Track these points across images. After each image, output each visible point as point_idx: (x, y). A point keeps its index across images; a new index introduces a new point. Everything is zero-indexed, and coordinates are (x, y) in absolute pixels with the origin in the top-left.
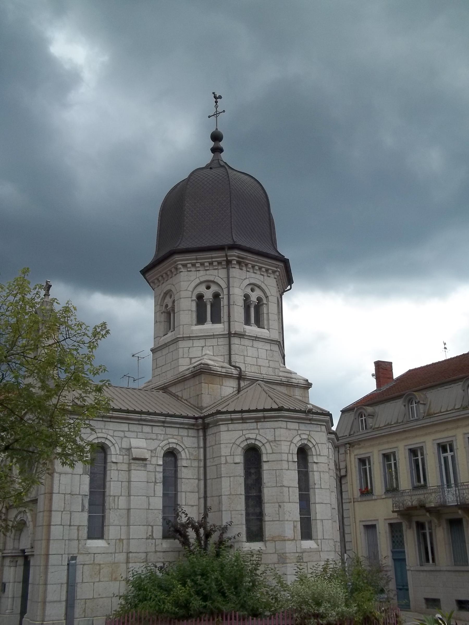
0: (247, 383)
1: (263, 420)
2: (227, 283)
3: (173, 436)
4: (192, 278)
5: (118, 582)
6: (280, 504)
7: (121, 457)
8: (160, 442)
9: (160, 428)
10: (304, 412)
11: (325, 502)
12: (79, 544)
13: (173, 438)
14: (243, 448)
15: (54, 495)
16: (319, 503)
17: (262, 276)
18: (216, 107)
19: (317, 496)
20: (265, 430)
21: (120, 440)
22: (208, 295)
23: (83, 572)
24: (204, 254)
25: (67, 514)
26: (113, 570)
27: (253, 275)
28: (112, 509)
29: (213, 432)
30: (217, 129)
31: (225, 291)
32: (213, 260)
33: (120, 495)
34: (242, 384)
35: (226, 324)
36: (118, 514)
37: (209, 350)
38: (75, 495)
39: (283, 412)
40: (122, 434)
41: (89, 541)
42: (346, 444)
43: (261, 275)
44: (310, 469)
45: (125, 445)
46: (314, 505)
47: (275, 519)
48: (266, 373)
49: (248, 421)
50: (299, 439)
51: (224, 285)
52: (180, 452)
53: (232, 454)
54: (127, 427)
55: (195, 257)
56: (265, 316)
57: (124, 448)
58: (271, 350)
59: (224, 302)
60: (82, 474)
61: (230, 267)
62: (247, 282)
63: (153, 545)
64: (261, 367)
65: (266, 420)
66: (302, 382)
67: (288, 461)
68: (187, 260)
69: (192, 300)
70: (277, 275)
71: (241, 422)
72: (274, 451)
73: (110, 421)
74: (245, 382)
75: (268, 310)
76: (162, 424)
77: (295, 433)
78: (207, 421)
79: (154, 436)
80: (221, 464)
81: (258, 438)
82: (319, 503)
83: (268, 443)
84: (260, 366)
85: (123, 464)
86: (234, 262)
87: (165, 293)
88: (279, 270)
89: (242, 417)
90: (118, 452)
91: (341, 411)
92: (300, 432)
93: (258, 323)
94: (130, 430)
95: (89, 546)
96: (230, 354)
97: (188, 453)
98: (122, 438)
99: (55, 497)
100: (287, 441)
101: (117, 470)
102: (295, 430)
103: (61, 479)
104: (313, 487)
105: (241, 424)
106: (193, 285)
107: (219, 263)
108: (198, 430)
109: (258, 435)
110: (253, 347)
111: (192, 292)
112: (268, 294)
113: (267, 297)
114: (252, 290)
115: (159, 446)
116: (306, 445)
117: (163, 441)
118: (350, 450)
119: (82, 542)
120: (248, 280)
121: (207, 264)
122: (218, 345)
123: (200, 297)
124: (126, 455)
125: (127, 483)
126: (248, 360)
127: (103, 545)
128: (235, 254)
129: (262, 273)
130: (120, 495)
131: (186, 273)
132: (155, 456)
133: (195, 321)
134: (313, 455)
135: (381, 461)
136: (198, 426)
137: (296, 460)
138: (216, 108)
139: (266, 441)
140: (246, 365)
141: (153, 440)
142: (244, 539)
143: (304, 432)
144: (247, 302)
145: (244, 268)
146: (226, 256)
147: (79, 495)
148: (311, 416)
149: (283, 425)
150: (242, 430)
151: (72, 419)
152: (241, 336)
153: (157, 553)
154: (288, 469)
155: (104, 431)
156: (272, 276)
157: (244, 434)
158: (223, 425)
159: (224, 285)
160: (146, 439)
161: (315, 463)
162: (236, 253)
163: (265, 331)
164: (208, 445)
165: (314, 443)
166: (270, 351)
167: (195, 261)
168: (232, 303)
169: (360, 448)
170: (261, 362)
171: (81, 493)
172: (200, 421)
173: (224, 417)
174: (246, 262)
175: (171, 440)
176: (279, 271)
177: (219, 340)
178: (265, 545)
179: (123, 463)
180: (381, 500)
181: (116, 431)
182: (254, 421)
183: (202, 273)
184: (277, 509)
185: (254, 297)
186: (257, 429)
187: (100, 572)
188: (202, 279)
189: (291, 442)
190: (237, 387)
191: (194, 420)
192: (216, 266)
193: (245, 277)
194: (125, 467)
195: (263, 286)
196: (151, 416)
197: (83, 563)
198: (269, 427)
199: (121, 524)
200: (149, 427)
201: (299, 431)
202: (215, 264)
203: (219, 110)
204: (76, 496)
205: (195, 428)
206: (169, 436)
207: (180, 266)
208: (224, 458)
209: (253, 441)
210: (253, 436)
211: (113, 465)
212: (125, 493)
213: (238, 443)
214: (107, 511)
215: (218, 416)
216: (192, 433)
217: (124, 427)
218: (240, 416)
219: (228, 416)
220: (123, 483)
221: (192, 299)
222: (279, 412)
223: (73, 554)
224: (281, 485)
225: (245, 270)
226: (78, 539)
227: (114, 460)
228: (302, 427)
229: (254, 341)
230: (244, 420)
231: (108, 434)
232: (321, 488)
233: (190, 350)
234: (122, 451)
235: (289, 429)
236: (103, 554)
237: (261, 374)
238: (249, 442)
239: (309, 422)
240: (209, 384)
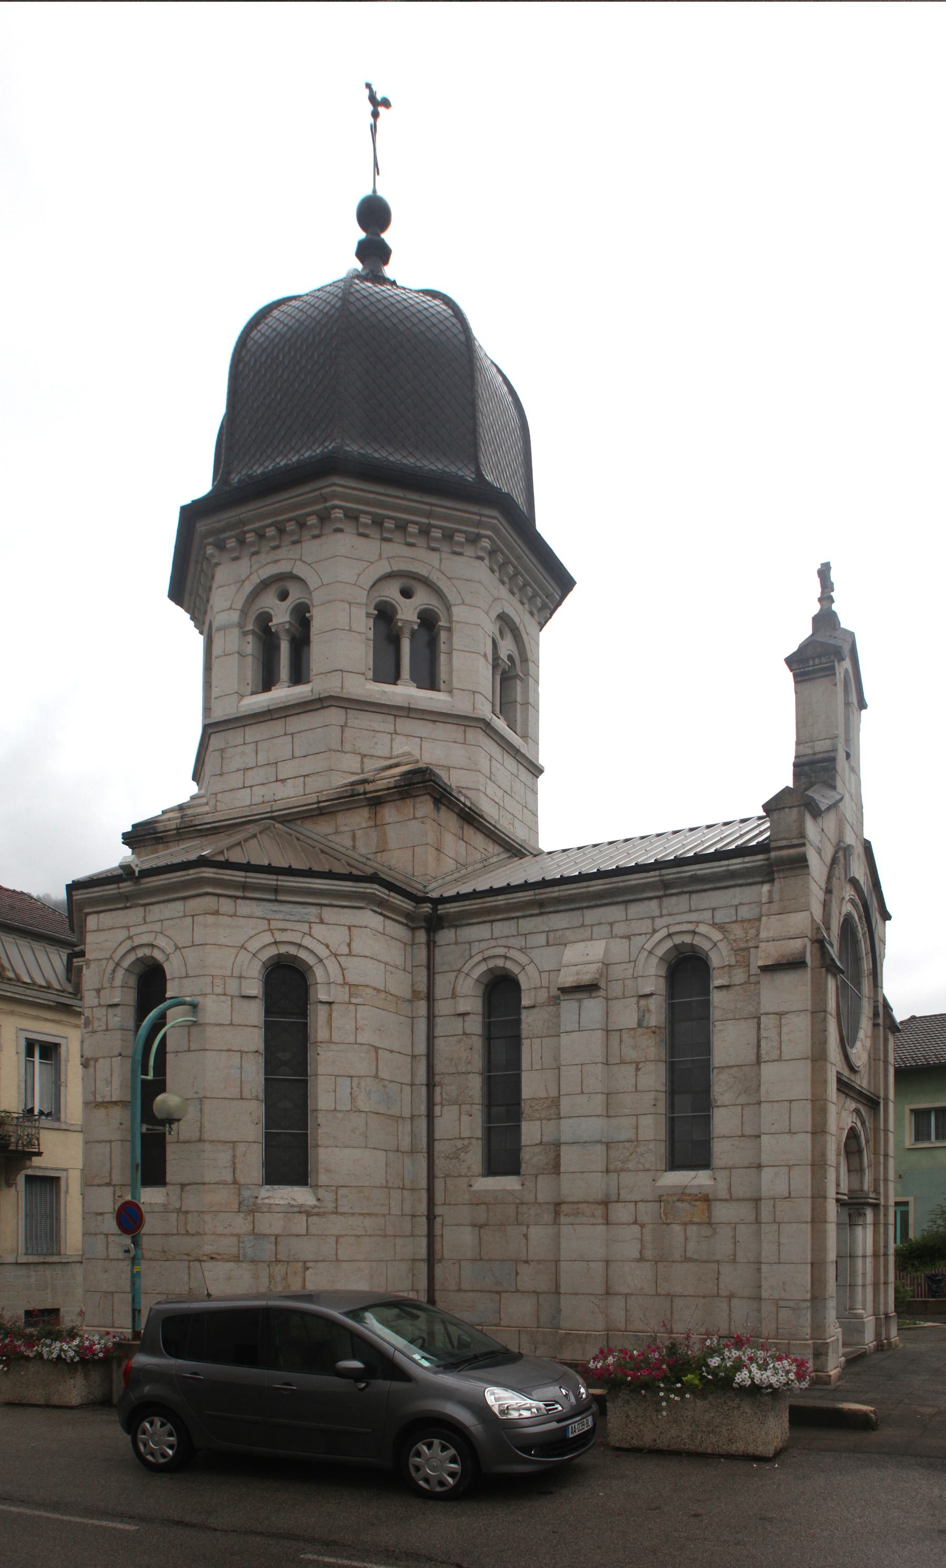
14: (661, 958)
22: (281, 616)
30: (374, 191)
50: (267, 938)
68: (367, 502)
69: (245, 634)
77: (263, 925)
78: (443, 909)
80: (126, 970)
111: (244, 612)
156: (469, 551)
172: (426, 908)
195: (435, 577)
225: (378, 536)
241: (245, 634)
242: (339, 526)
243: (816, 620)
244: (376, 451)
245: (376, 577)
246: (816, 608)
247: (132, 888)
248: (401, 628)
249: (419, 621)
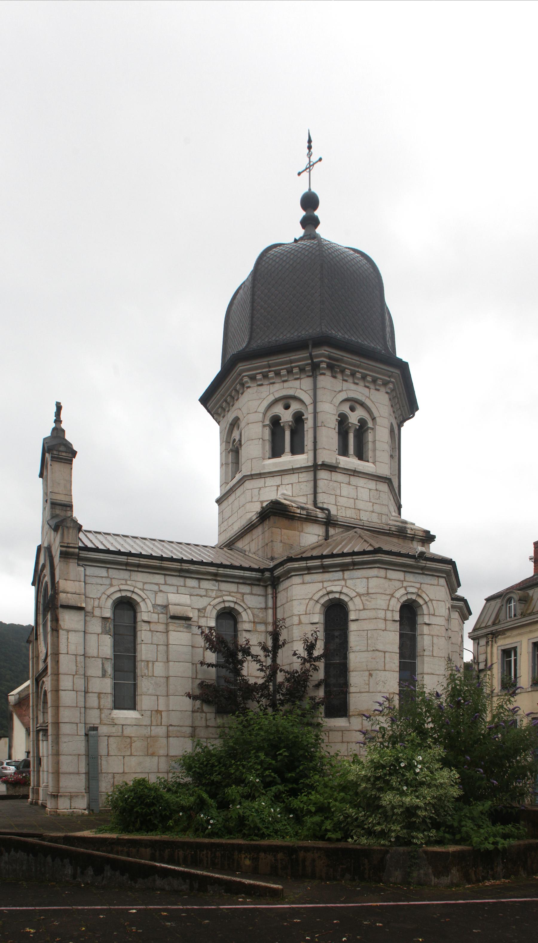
0: (338, 530)
1: (352, 568)
2: (312, 397)
3: (230, 594)
4: (264, 395)
5: (157, 758)
6: (370, 672)
7: (156, 616)
8: (211, 599)
9: (211, 582)
10: (413, 557)
11: (438, 673)
12: (101, 713)
13: (230, 595)
14: (322, 605)
15: (61, 657)
16: (428, 674)
17: (367, 390)
18: (310, 155)
19: (425, 665)
20: (354, 580)
21: (154, 595)
22: (287, 417)
23: (108, 745)
24: (280, 357)
25: (80, 678)
26: (148, 744)
27: (353, 387)
28: (145, 675)
29: (284, 588)
30: (310, 189)
31: (311, 408)
32: (293, 365)
33: (155, 660)
34: (332, 531)
35: (311, 454)
36: (153, 682)
37: (287, 490)
38: (92, 657)
39: (380, 555)
40: (156, 588)
41: (116, 712)
42: (488, 634)
43: (366, 386)
44: (418, 632)
45: (160, 600)
46: (421, 676)
47: (363, 690)
48: (368, 519)
49: (330, 570)
50: (403, 591)
51: (307, 399)
52: (239, 613)
53: (308, 612)
54: (163, 579)
55: (266, 363)
56: (370, 445)
57: (159, 605)
58: (377, 490)
59: (309, 425)
60: (101, 634)
61: (318, 373)
62: (343, 396)
63: (203, 719)
64: (361, 511)
65: (355, 567)
66: (421, 534)
67: (385, 620)
70: (390, 388)
71: (321, 571)
72: (366, 607)
73: (138, 571)
74: (337, 529)
75: (375, 436)
76: (214, 578)
77: (398, 584)
78: (277, 573)
79: (203, 592)
81: (345, 590)
82: (428, 674)
83: (358, 597)
84: (359, 510)
85: (158, 624)
86: (324, 365)
87: (231, 424)
88: (393, 380)
89: (322, 564)
90: (151, 609)
91: (485, 600)
92: (405, 584)
93: (360, 455)
94: (168, 583)
95: (115, 716)
96: (315, 493)
97: (251, 615)
98: (156, 593)
99: (63, 659)
100: (385, 594)
101: (150, 630)
102: (399, 580)
103: (69, 637)
104: (421, 654)
105: (320, 575)
106: (265, 404)
107: (302, 370)
108: (266, 587)
109: (344, 588)
110: (349, 484)
111: (265, 414)
112: (376, 414)
113: (374, 419)
114: (352, 409)
115: (209, 604)
116: (415, 601)
117: (215, 598)
118: (492, 641)
119: (106, 712)
120: (344, 393)
121: (284, 372)
122: (299, 482)
123: (276, 422)
124: (162, 613)
125: (165, 647)
126: (342, 501)
127: (134, 717)
128: (323, 352)
129: (367, 384)
130: (155, 660)
131: (255, 389)
132: (204, 617)
133: (268, 454)
134: (423, 614)
135: (531, 650)
136: (266, 582)
137: (398, 618)
138: (309, 158)
139: (355, 594)
140: (339, 508)
141: (201, 596)
142: (323, 715)
143: (413, 584)
144: (344, 426)
145: (339, 376)
146: (311, 357)
147: (98, 657)
148: (423, 563)
149: (382, 573)
150: (323, 582)
151: (82, 566)
152: (332, 468)
153: (209, 728)
154: (385, 630)
155: (129, 582)
156: (383, 389)
157: (325, 586)
158: (297, 577)
159: (307, 399)
160: (191, 595)
161: (426, 624)
162: (324, 351)
163: (370, 465)
164: (279, 604)
165: (427, 599)
166: (375, 491)
167: (267, 370)
168: (319, 424)
169: (505, 638)
170: (361, 505)
171: (100, 655)
172: (267, 574)
173: (297, 566)
174: (341, 366)
175: (226, 598)
176: (392, 382)
177: (301, 475)
178: (349, 721)
179: (159, 622)
180: (526, 694)
181: (146, 583)
182: (339, 569)
183: (277, 386)
184: (366, 678)
185: (354, 418)
186: (344, 579)
187: (131, 746)
188: (278, 395)
189: (392, 596)
190: (324, 535)
191: (260, 574)
192: (297, 374)
193: (340, 389)
194: (161, 628)
195: (368, 403)
196: (196, 566)
197: (108, 735)
198: (360, 576)
199: (158, 693)
200: (194, 580)
201: (404, 582)
202: (296, 370)
203: (314, 159)
204: (94, 659)
205: (262, 584)
206: (224, 593)
207: (246, 379)
208: (298, 618)
209: (337, 596)
210: (337, 589)
211: (143, 624)
212: (162, 657)
213: (316, 598)
214: (139, 679)
215: (288, 564)
216: (257, 590)
217: (159, 579)
218: (320, 563)
219: (303, 564)
220: (159, 647)
221: (265, 424)
222: (374, 555)
223: (94, 724)
224: (374, 649)
225: (341, 378)
226: (99, 708)
227: (146, 618)
228: (410, 577)
229: (352, 477)
230: (325, 569)
231: (135, 587)
232: (433, 656)
233: (261, 492)
234: (156, 609)
235: (390, 579)
236: (135, 726)
237: (361, 520)
238: (331, 596)
239: (421, 572)
240: (282, 530)
241: (264, 426)
242: (324, 372)
243: (54, 429)
244: (336, 332)
245: (341, 400)
246: (54, 425)
247: (414, 563)
248: (350, 427)
249: (359, 424)
